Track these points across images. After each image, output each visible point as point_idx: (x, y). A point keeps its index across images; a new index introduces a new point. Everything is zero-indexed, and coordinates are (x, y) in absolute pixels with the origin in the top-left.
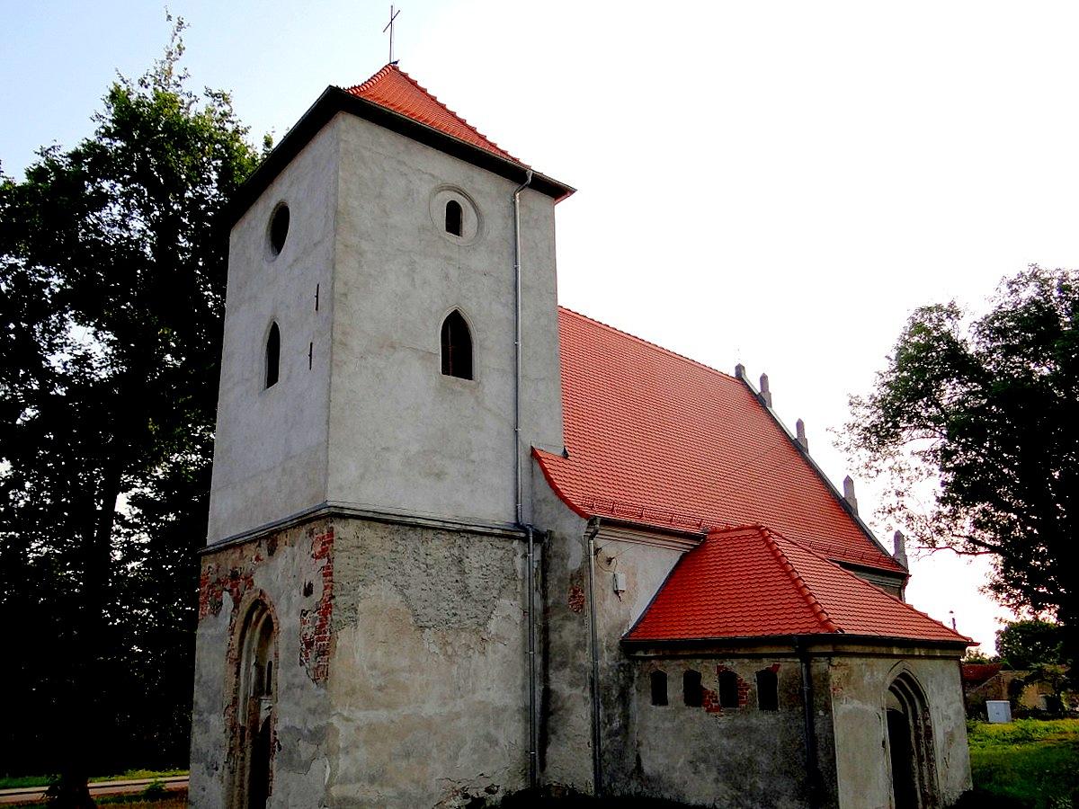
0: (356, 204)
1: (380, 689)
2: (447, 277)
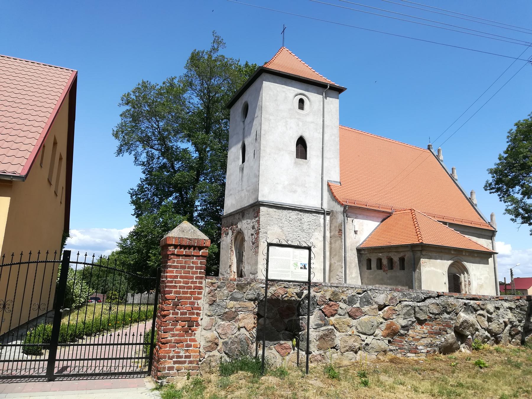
0: (268, 104)
2: (298, 125)
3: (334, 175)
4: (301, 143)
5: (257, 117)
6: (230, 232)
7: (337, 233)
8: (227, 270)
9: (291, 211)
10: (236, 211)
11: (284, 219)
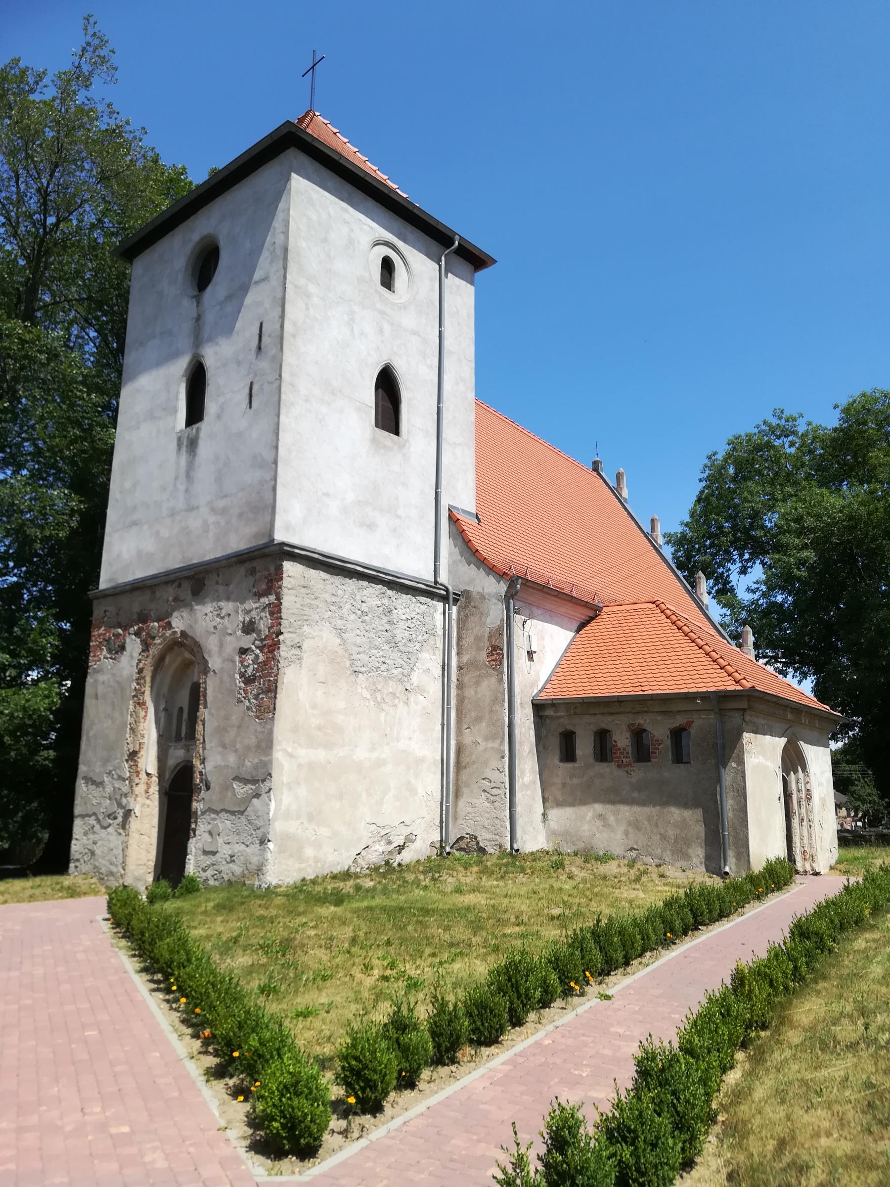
0: (304, 245)
1: (319, 728)
2: (381, 331)
3: (462, 495)
4: (387, 385)
5: (265, 279)
6: (134, 645)
7: (483, 656)
8: (119, 767)
9: (365, 583)
10: (167, 574)
11: (348, 606)
